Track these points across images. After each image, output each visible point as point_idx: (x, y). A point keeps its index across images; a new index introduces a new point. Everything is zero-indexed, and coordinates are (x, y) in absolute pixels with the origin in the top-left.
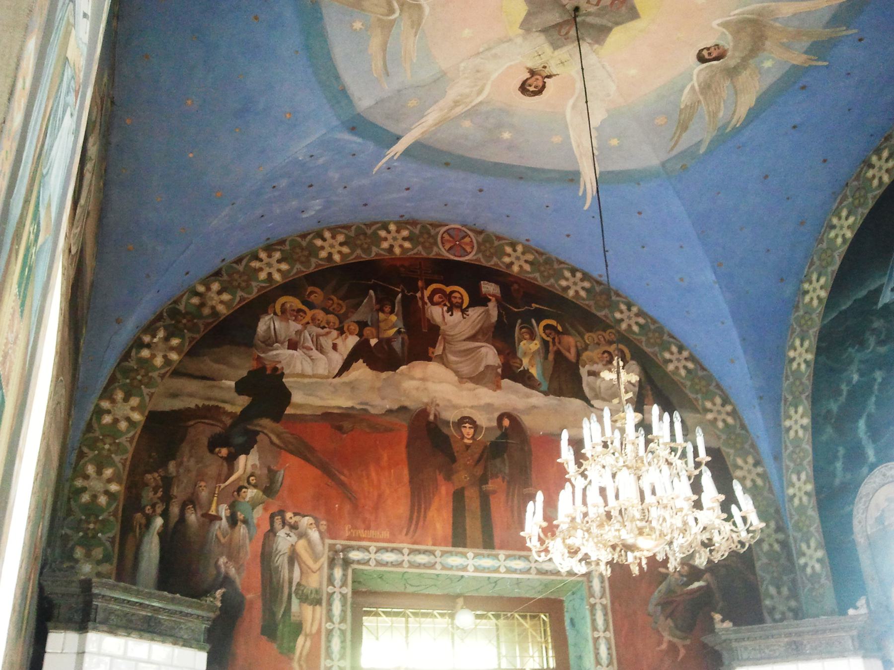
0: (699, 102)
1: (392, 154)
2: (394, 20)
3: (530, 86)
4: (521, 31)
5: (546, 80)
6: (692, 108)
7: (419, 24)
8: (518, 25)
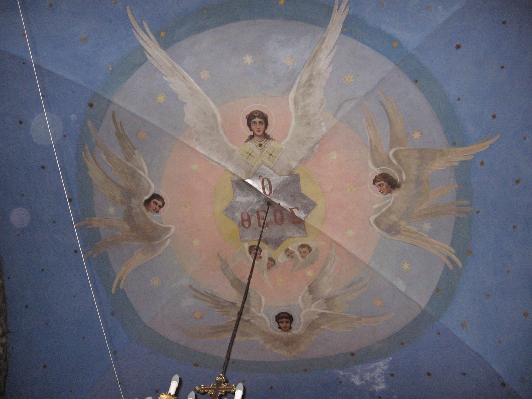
0: (128, 160)
1: (343, 6)
2: (391, 148)
3: (260, 122)
4: (296, 172)
5: (252, 133)
6: (129, 157)
7: (371, 151)
8: (301, 176)
